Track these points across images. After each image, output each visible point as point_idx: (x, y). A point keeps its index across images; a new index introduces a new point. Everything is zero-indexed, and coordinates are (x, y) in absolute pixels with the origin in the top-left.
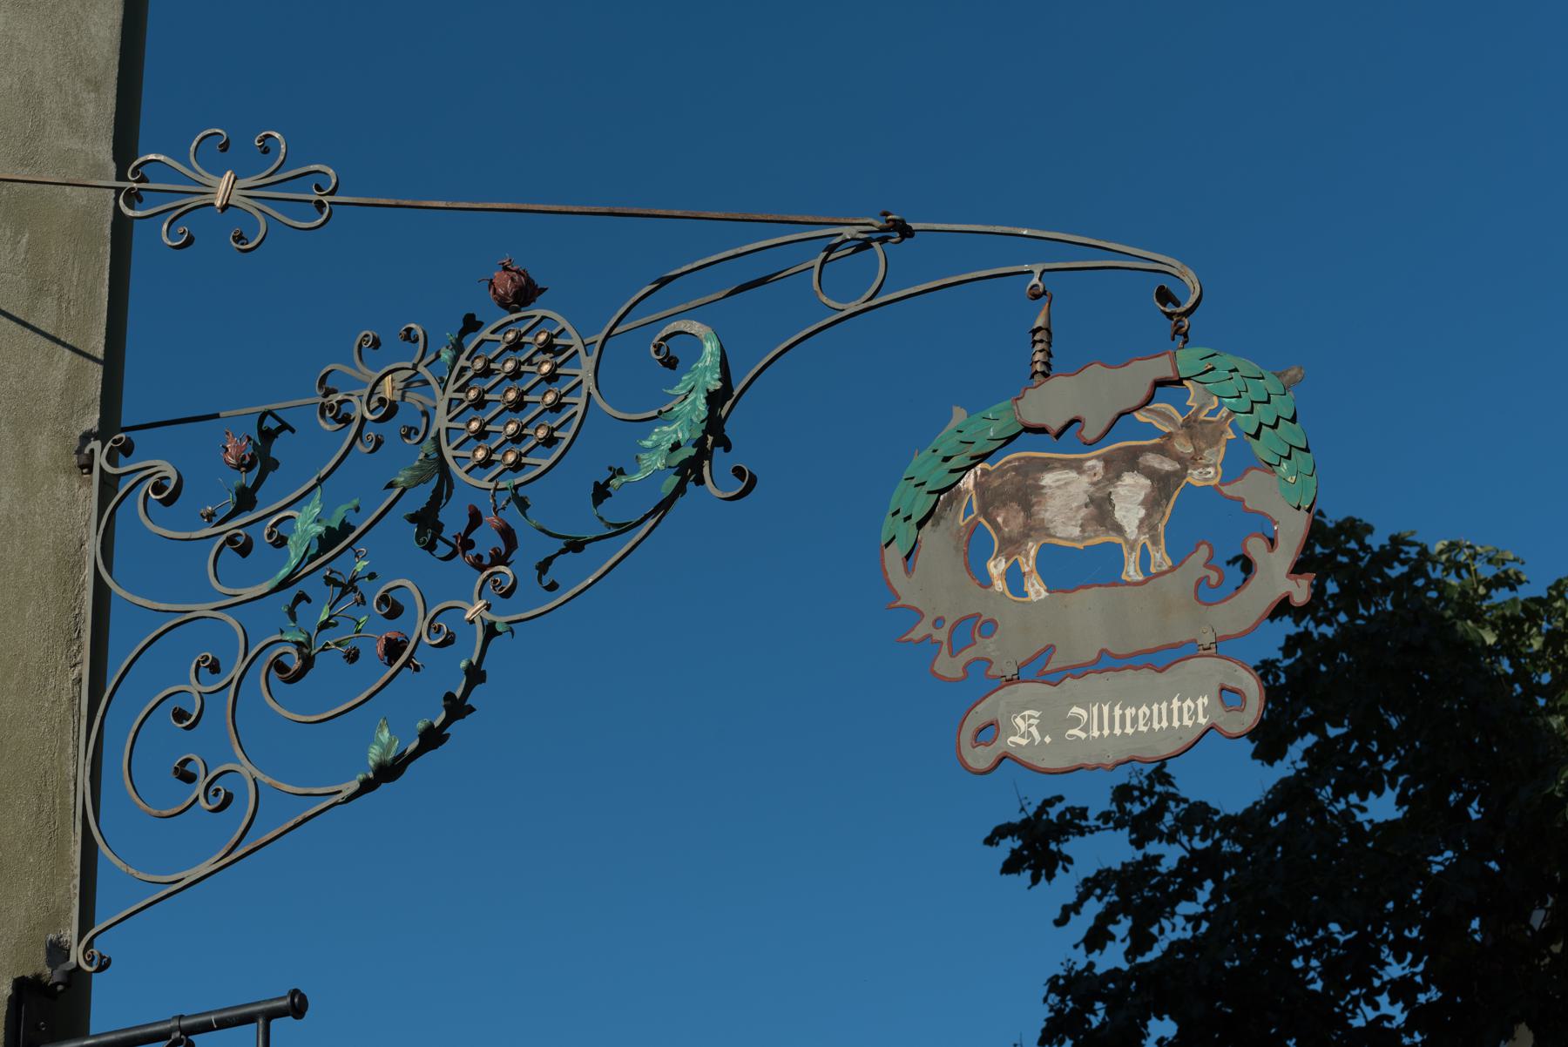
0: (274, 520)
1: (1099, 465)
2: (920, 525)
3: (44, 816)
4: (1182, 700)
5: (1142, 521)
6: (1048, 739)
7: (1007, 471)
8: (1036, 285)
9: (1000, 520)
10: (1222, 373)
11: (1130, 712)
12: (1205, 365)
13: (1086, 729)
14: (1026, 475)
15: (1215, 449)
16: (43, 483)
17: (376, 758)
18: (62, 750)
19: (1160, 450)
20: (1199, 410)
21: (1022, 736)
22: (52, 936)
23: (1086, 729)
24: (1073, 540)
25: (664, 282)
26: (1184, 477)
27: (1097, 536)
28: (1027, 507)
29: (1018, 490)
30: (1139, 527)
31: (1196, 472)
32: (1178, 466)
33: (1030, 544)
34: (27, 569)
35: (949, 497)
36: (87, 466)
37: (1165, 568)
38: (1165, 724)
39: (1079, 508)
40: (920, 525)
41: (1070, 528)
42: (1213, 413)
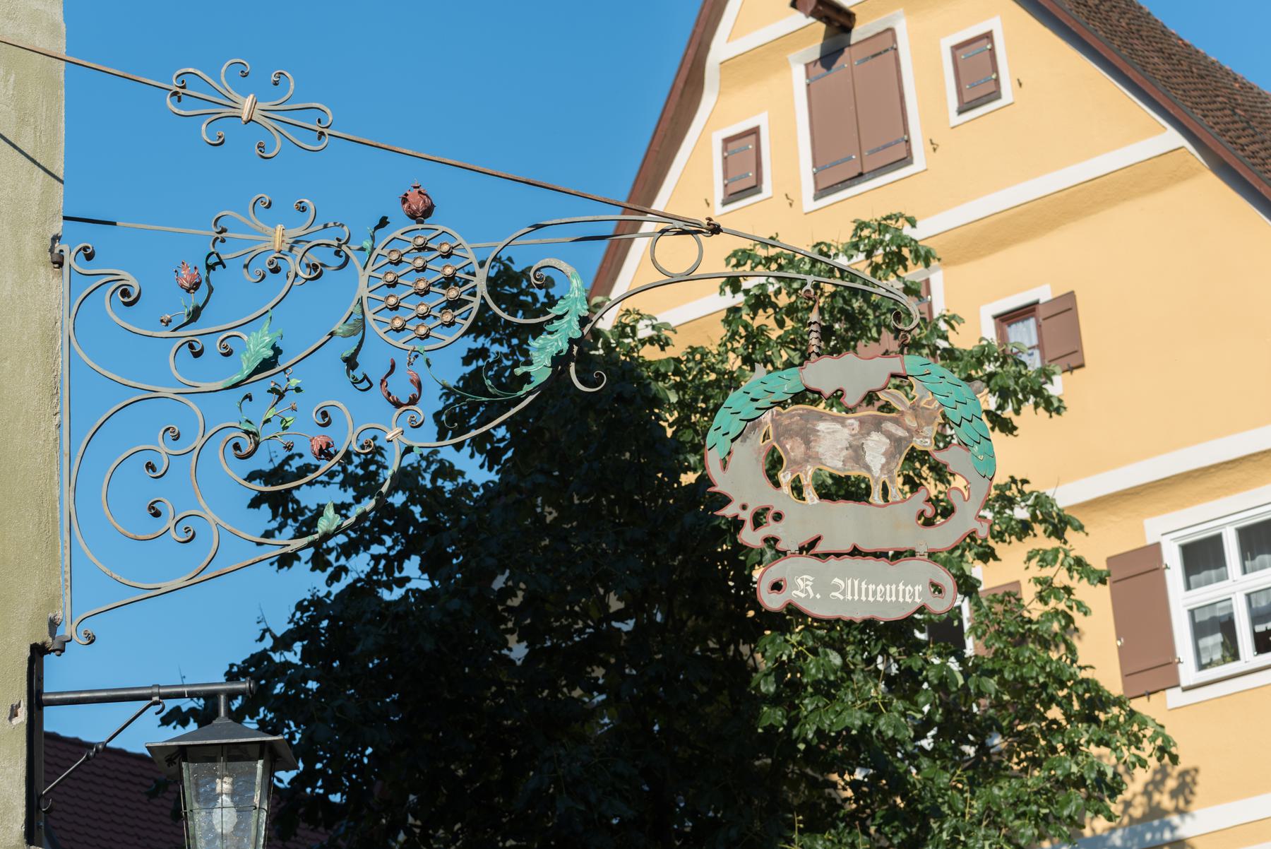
0: (225, 335)
1: (856, 424)
2: (733, 440)
3: (42, 526)
4: (905, 584)
5: (883, 466)
6: (818, 596)
7: (794, 416)
8: (808, 291)
9: (788, 447)
10: (935, 377)
11: (872, 587)
12: (924, 370)
13: (843, 593)
14: (807, 421)
15: (931, 427)
16: (31, 273)
17: (325, 529)
18: (52, 478)
19: (896, 422)
20: (921, 399)
21: (802, 591)
22: (51, 615)
23: (843, 593)
24: (838, 470)
25: (538, 227)
26: (911, 442)
27: (853, 470)
28: (807, 442)
29: (801, 429)
30: (882, 469)
31: (918, 440)
32: (907, 434)
33: (809, 467)
34: (25, 338)
35: (754, 425)
36: (59, 263)
37: (898, 499)
38: (894, 599)
39: (842, 449)
40: (733, 440)
41: (835, 461)
42: (929, 403)
